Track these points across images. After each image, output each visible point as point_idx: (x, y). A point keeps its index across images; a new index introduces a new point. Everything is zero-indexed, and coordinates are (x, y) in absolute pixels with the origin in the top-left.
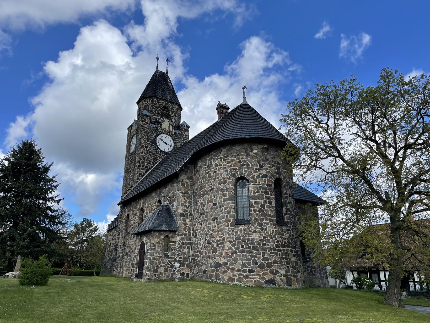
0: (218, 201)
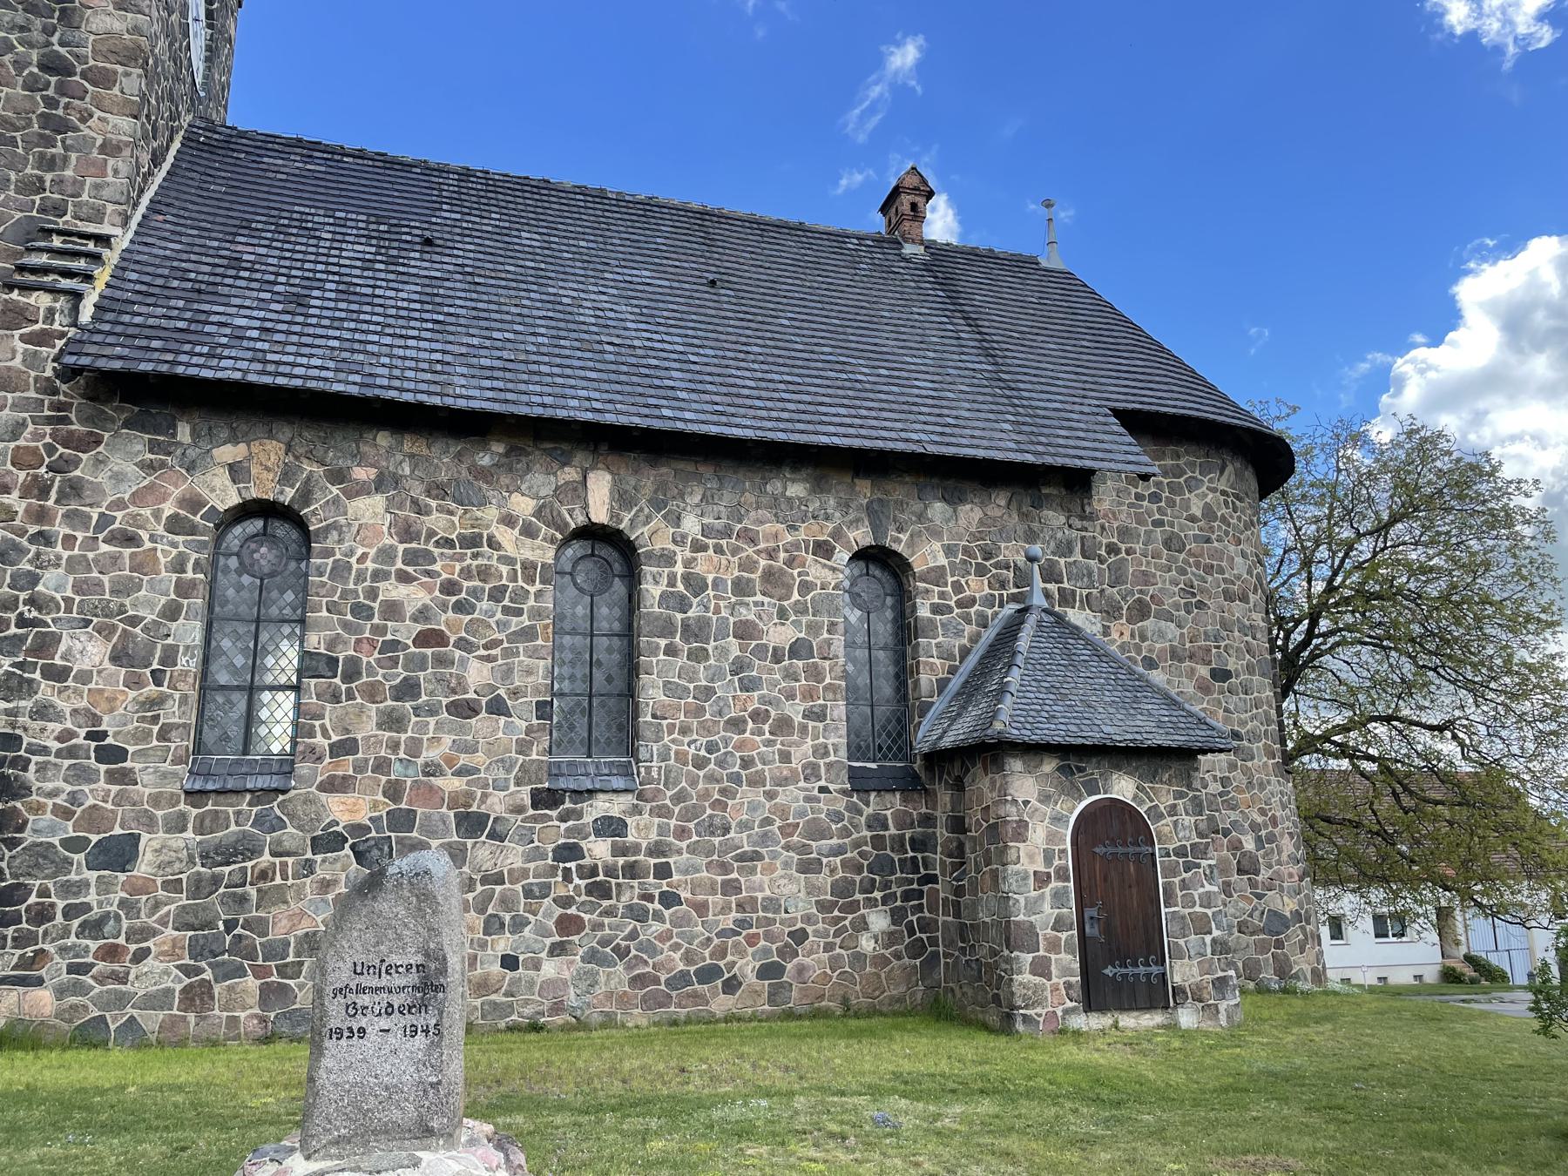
0: (1232, 664)
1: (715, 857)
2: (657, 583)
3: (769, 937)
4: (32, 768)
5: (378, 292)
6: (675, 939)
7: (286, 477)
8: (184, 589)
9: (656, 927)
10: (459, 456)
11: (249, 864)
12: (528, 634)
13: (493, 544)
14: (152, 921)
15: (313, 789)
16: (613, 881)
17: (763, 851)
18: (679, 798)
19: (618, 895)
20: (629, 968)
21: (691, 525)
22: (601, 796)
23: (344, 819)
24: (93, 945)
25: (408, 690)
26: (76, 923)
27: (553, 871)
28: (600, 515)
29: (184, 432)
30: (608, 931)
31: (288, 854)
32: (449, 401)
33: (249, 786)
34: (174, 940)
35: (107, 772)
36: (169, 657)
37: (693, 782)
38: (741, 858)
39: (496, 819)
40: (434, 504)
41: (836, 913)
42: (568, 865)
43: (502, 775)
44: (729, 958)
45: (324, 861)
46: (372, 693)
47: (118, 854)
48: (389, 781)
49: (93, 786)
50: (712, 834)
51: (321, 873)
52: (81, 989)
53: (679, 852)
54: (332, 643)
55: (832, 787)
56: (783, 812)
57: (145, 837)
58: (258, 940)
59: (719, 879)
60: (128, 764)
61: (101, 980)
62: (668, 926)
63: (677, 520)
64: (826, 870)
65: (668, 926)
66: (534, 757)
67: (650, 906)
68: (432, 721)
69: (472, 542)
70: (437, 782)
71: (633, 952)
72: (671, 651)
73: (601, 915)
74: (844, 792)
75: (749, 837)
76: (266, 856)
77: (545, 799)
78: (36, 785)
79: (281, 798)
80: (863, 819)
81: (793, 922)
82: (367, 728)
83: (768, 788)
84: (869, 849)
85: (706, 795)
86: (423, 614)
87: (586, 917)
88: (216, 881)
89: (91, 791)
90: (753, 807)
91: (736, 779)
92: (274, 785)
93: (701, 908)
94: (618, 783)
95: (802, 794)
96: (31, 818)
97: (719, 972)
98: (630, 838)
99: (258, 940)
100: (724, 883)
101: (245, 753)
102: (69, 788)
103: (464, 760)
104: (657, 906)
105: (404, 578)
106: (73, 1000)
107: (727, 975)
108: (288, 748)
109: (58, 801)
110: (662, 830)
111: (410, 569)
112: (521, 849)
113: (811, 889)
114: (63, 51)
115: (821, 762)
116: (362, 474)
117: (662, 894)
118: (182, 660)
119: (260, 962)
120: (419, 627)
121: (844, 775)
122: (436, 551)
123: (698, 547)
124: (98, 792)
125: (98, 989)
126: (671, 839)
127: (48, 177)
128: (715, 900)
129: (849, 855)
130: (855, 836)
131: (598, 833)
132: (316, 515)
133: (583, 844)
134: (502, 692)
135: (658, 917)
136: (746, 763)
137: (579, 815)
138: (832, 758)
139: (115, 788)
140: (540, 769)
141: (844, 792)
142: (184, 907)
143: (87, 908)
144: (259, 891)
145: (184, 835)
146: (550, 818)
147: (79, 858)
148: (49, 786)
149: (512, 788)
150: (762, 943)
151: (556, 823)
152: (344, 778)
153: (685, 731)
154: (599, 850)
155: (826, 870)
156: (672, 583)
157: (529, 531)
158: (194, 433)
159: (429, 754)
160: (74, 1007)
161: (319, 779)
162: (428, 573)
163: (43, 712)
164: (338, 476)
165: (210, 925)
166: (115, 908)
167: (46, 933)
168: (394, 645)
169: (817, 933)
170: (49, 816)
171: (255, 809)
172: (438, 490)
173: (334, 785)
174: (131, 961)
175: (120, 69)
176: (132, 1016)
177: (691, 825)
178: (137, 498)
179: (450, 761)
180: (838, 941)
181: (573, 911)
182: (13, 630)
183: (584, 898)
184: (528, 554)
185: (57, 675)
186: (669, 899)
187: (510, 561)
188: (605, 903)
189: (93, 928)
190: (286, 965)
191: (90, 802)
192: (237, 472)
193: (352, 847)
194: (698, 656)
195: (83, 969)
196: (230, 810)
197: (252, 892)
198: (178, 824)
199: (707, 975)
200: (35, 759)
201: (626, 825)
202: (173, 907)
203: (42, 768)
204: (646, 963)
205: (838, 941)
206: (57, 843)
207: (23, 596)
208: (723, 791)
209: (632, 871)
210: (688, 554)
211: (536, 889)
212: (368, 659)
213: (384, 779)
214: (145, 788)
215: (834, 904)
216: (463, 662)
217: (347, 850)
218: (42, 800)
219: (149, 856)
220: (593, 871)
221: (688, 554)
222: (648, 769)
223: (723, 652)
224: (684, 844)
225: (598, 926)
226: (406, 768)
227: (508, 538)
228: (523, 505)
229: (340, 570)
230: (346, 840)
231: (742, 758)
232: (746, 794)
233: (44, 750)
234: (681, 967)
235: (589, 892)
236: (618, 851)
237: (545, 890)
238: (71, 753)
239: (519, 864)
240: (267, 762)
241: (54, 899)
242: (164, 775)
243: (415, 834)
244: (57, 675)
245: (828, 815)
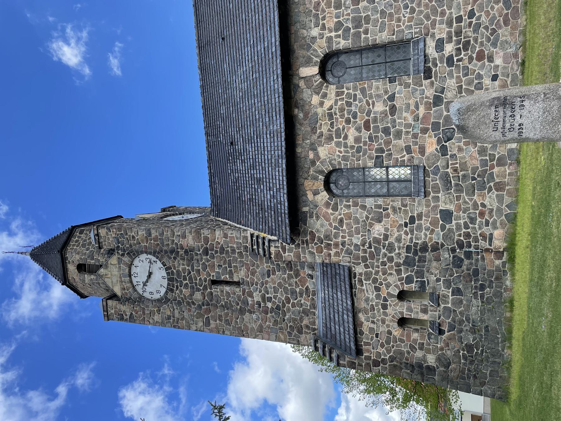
2: (339, 43)
5: (251, 157)
7: (316, 179)
8: (356, 204)
9: (483, 18)
10: (301, 124)
12: (363, 91)
13: (331, 108)
18: (427, 17)
21: (315, 32)
24: (479, 219)
25: (386, 131)
26: (471, 225)
28: (315, 70)
29: (305, 209)
32: (283, 130)
36: (379, 207)
37: (421, 12)
40: (318, 131)
46: (388, 143)
47: (447, 215)
51: (455, 152)
54: (371, 158)
57: (441, 208)
61: (491, 216)
63: (314, 38)
68: (398, 121)
69: (331, 116)
72: (366, 32)
77: (428, 74)
82: (401, 143)
86: (358, 129)
88: (457, 185)
103: (412, 107)
105: (346, 137)
106: (498, 224)
110: (441, 22)
111: (342, 136)
114: (201, 251)
116: (311, 155)
118: (379, 203)
120: (363, 130)
122: (335, 128)
123: (324, 27)
124: (425, 223)
127: (237, 251)
132: (327, 168)
134: (386, 97)
135: (479, 18)
143: (465, 223)
148: (423, 236)
153: (399, 20)
154: (449, 48)
156: (338, 36)
157: (325, 96)
158: (306, 206)
159: (410, 120)
162: (343, 129)
163: (399, 240)
164: (313, 163)
165: (473, 186)
168: (370, 138)
172: (314, 130)
173: (422, 151)
175: (202, 235)
178: (328, 220)
179: (413, 112)
181: (474, 56)
182: (373, 250)
184: (333, 95)
185: (386, 237)
186: (471, 14)
187: (336, 102)
189: (473, 220)
192: (316, 193)
194: (367, 19)
197: (461, 174)
198: (437, 199)
203: (417, 239)
207: (362, 248)
209: (458, 33)
210: (327, 31)
212: (376, 145)
214: (424, 210)
216: (375, 113)
221: (327, 31)
223: (366, 9)
224: (448, 12)
225: (482, 44)
227: (328, 104)
228: (315, 99)
229: (345, 158)
233: (411, 239)
236: (450, 40)
238: (412, 231)
242: (419, 204)
243: (441, 121)
244: (386, 237)
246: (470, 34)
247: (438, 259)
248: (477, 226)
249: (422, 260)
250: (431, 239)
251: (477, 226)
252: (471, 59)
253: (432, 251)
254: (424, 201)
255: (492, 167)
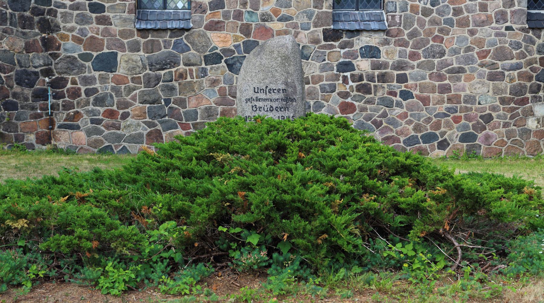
1: (435, 71)
3: (467, 118)
4: (59, 15)
6: (409, 118)
9: (398, 111)
11: (173, 70)
14: (128, 99)
15: (202, 29)
16: (372, 84)
17: (466, 67)
18: (412, 35)
19: (375, 92)
20: (382, 133)
22: (365, 34)
23: (220, 46)
24: (102, 110)
26: (92, 99)
27: (337, 78)
30: (369, 112)
31: (193, 65)
33: (169, 26)
34: (141, 108)
35: (96, 18)
37: (422, 24)
38: (451, 71)
39: (303, 47)
41: (512, 105)
42: (345, 74)
43: (306, 20)
44: (443, 129)
45: (211, 69)
47: (108, 63)
48: (242, 25)
49: (91, 26)
50: (434, 57)
51: (211, 75)
52: (100, 132)
53: (413, 68)
55: (514, 26)
56: (480, 43)
57: (120, 54)
58: (182, 111)
59: (437, 84)
60: (106, 14)
61: (108, 127)
62: (405, 110)
64: (507, 79)
65: (405, 110)
66: (324, 10)
67: (394, 98)
70: (268, 24)
71: (384, 124)
73: (365, 103)
74: (523, 30)
75: (457, 58)
76: (182, 66)
77: (332, 35)
78: (62, 25)
79: (186, 33)
80: (535, 47)
81: (484, 109)
83: (471, 28)
84: (537, 66)
85: (430, 33)
87: (357, 104)
89: (90, 28)
90: (461, 40)
91: (449, 22)
92: (182, 26)
93: (425, 101)
94: (374, 26)
95: (494, 32)
96: (62, 42)
97: (435, 137)
98: (382, 59)
99: (182, 111)
100: (440, 86)
101: (165, 8)
102: (78, 27)
103: (284, 11)
104: (398, 98)
106: (95, 137)
107: (440, 139)
108: (186, 5)
109: (74, 33)
112: (318, 64)
113: (497, 91)
115: (508, 11)
117: (401, 92)
119: (184, 122)
121: (524, 18)
124: (93, 29)
125: (106, 132)
126: (407, 60)
128: (434, 96)
129: (524, 69)
130: (529, 57)
131: (363, 56)
133: (354, 62)
135: (399, 105)
136: (457, 12)
137: (351, 45)
138: (516, 7)
139: (101, 27)
140: (327, 17)
141: (523, 30)
142: (143, 91)
143: (95, 91)
144: (180, 84)
145: (139, 53)
146: (334, 47)
147: (89, 64)
148: (69, 25)
149: (312, 29)
150: (463, 121)
151: (338, 49)
152: (218, 22)
154: (363, 65)
155: (507, 79)
160: (96, 141)
161: (205, 23)
166: (109, 91)
167: (78, 103)
169: (499, 117)
170: (70, 41)
171: (173, 40)
173: (215, 26)
174: (121, 118)
176: (124, 146)
177: (420, 51)
179: (276, 12)
180: (512, 122)
181: (349, 100)
183: (355, 93)
186: (406, 95)
188: (368, 96)
189: (100, 101)
190: (197, 124)
191: (90, 35)
193: (226, 61)
195: (99, 122)
196: (161, 40)
197: (176, 84)
198: (135, 48)
199: (429, 138)
200: (60, 10)
201: (380, 51)
202: (138, 91)
203: (64, 15)
204: (392, 130)
205: (512, 122)
206: (77, 56)
208: (441, 31)
209: (383, 78)
211: (327, 87)
213: (240, 23)
214: (116, 28)
215: (511, 100)
217: (223, 64)
218: (66, 33)
219: (123, 64)
220: (361, 78)
222: (393, 17)
224: (415, 63)
225: (363, 109)
226: (251, 16)
230: (222, 58)
231: (454, 9)
232: (457, 32)
233: (64, 6)
234: (413, 133)
235: (358, 90)
236: (375, 66)
237: (333, 89)
239: (317, 73)
240: (176, 14)
241: (79, 86)
242: (125, 20)
245: (511, 45)
246: (380, 94)
247: (28, 48)
248: (91, 107)
249: (26, 23)
250: (64, 38)
251: (91, 107)
252: (345, 95)
253: (43, 39)
254: (130, 27)
255: (185, 127)
